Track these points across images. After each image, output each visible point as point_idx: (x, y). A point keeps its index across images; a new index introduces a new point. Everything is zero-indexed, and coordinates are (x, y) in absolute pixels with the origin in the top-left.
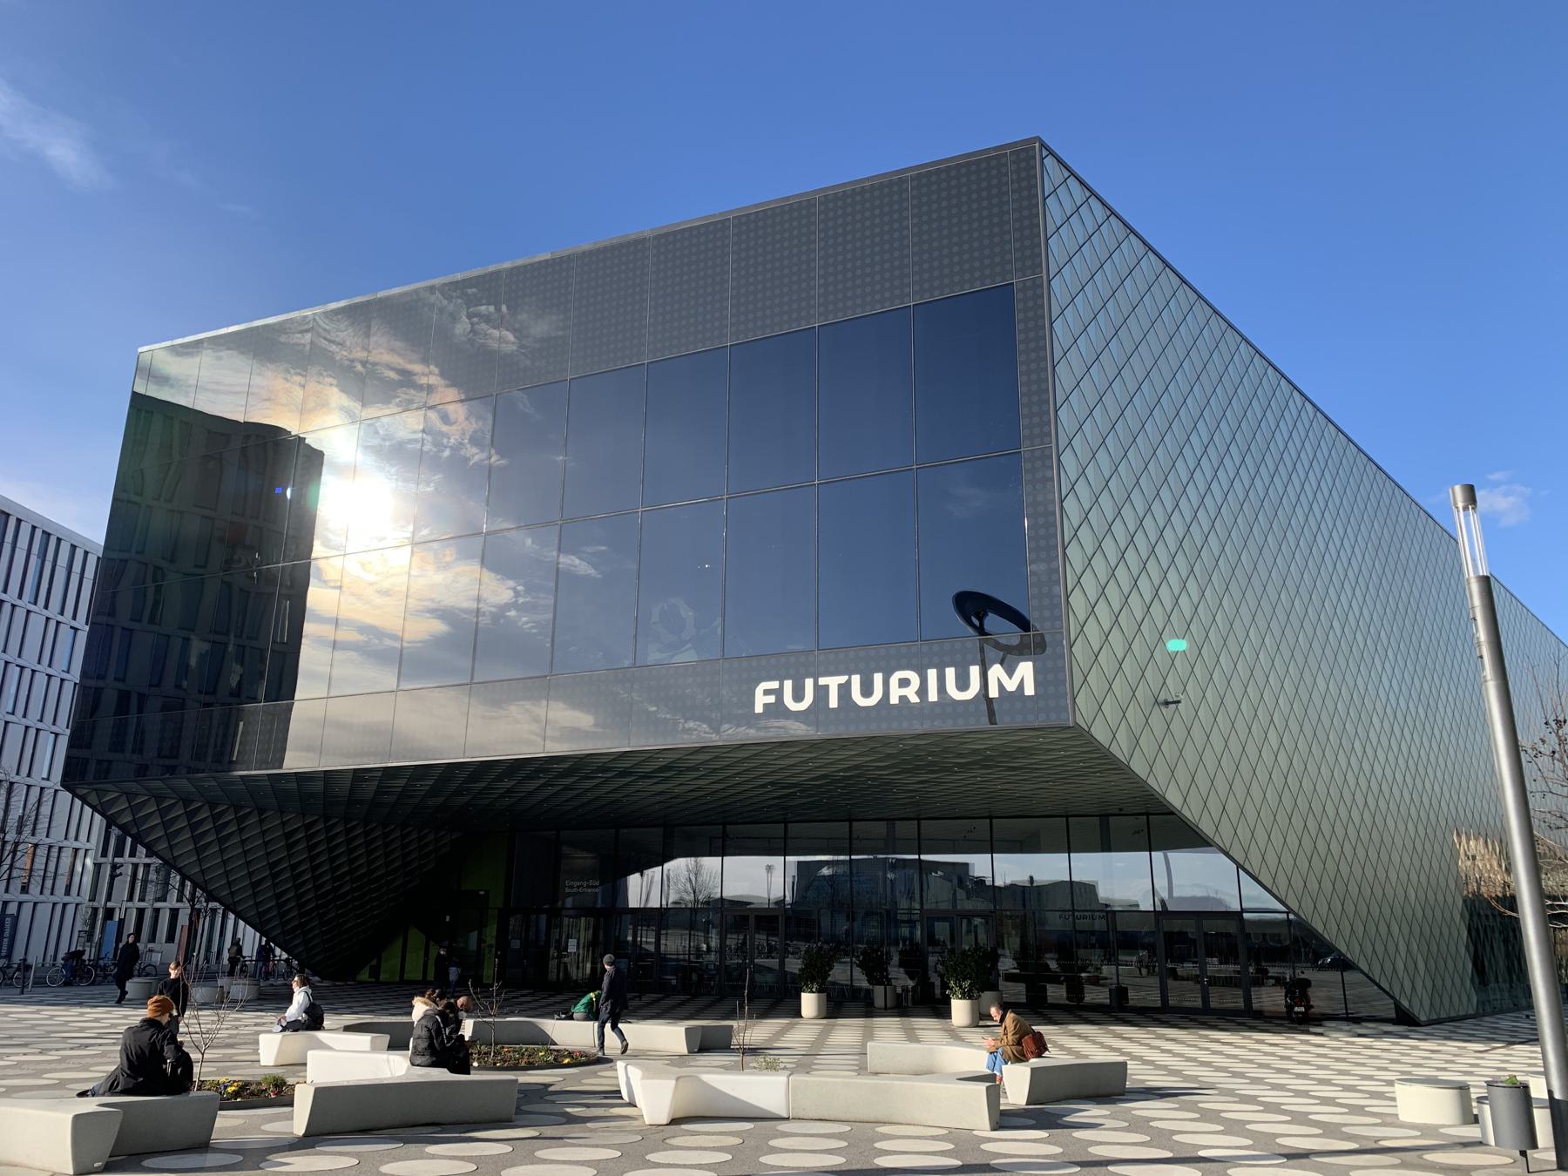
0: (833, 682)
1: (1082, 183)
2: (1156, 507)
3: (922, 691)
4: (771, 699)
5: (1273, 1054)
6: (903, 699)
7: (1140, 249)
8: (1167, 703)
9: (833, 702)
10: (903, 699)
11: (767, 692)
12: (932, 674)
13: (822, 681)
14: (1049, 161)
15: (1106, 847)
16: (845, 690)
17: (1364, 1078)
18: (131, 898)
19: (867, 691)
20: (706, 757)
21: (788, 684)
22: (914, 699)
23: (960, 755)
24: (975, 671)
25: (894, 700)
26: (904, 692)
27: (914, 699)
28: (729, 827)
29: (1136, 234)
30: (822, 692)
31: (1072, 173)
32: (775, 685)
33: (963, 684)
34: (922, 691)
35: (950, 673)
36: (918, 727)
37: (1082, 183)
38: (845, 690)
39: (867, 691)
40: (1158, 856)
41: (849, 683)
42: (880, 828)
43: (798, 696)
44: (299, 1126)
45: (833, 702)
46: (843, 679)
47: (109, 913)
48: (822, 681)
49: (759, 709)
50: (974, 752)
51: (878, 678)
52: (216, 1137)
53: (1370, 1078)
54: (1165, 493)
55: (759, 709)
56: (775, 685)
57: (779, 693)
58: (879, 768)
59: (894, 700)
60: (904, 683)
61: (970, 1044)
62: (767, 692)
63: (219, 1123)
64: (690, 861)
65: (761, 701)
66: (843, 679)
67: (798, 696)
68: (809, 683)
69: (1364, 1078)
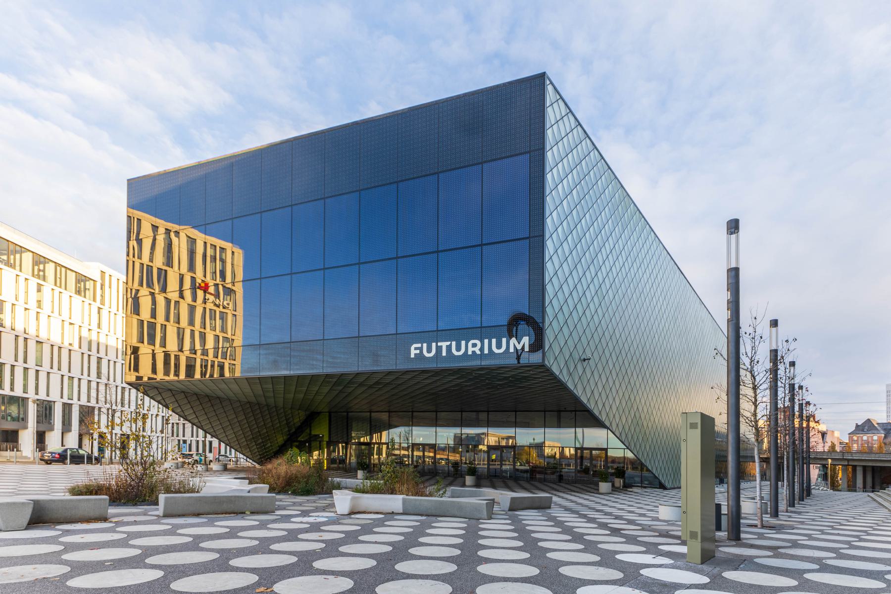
0: (444, 345)
1: (566, 104)
2: (587, 273)
3: (482, 349)
4: (418, 352)
5: (614, 507)
6: (474, 352)
7: (591, 147)
8: (584, 360)
9: (444, 354)
10: (474, 352)
11: (416, 349)
12: (486, 341)
13: (439, 344)
14: (550, 88)
15: (559, 426)
16: (449, 348)
17: (649, 510)
18: (192, 436)
19: (458, 349)
20: (393, 377)
21: (425, 345)
22: (478, 352)
23: (500, 380)
24: (504, 340)
25: (470, 353)
26: (474, 349)
27: (478, 352)
28: (373, 414)
29: (590, 139)
30: (439, 349)
31: (561, 98)
32: (419, 345)
33: (499, 346)
34: (482, 349)
35: (494, 341)
36: (476, 363)
37: (566, 104)
38: (449, 348)
39: (458, 349)
40: (579, 430)
41: (451, 345)
42: (473, 415)
43: (429, 351)
44: (160, 512)
45: (444, 354)
46: (448, 343)
47: (185, 442)
48: (439, 344)
49: (412, 356)
50: (505, 378)
51: (463, 343)
52: (717, 554)
53: (644, 515)
54: (592, 267)
55: (412, 356)
56: (419, 345)
57: (421, 349)
58: (466, 386)
59: (470, 353)
60: (474, 345)
61: (128, 325)
62: (416, 349)
63: (109, 511)
64: (407, 429)
65: (413, 352)
66: (448, 343)
67: (429, 351)
68: (434, 345)
69: (649, 510)
